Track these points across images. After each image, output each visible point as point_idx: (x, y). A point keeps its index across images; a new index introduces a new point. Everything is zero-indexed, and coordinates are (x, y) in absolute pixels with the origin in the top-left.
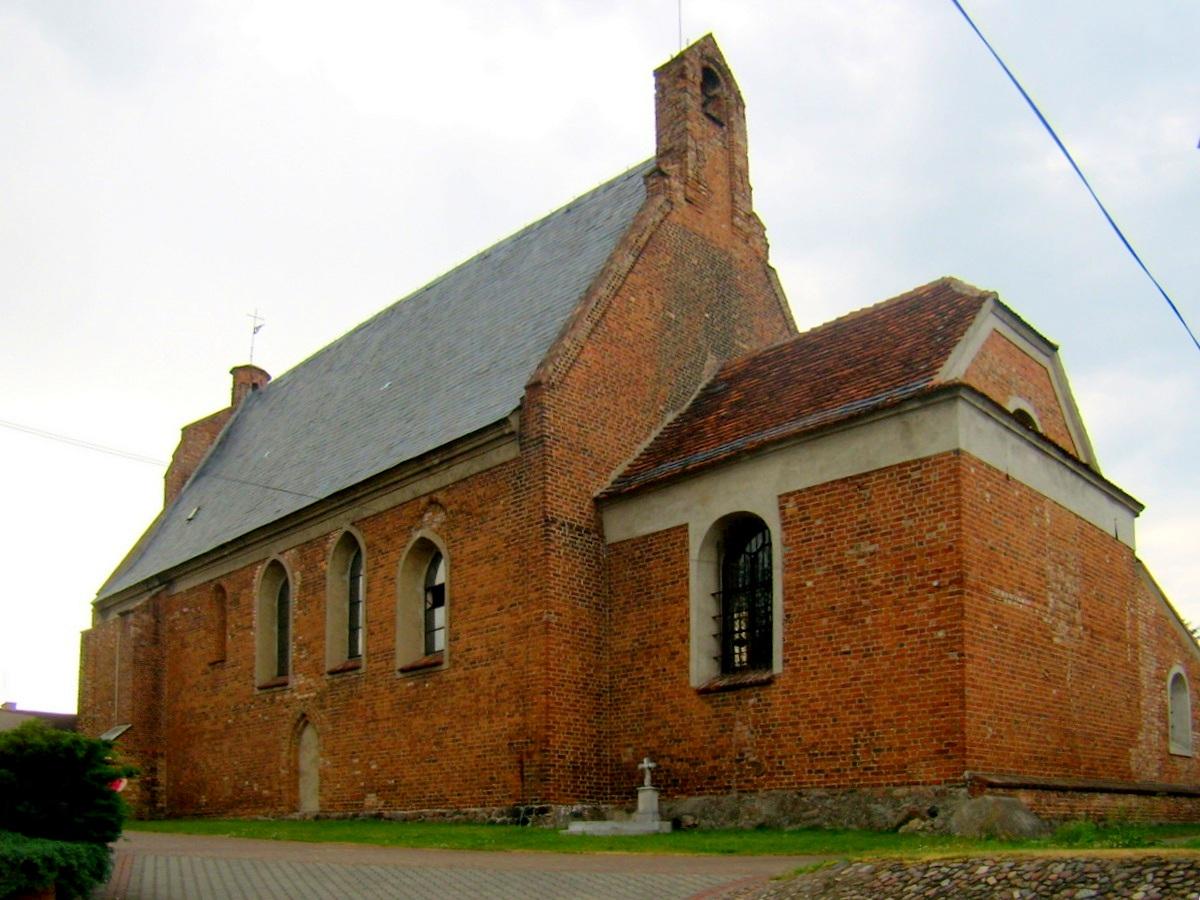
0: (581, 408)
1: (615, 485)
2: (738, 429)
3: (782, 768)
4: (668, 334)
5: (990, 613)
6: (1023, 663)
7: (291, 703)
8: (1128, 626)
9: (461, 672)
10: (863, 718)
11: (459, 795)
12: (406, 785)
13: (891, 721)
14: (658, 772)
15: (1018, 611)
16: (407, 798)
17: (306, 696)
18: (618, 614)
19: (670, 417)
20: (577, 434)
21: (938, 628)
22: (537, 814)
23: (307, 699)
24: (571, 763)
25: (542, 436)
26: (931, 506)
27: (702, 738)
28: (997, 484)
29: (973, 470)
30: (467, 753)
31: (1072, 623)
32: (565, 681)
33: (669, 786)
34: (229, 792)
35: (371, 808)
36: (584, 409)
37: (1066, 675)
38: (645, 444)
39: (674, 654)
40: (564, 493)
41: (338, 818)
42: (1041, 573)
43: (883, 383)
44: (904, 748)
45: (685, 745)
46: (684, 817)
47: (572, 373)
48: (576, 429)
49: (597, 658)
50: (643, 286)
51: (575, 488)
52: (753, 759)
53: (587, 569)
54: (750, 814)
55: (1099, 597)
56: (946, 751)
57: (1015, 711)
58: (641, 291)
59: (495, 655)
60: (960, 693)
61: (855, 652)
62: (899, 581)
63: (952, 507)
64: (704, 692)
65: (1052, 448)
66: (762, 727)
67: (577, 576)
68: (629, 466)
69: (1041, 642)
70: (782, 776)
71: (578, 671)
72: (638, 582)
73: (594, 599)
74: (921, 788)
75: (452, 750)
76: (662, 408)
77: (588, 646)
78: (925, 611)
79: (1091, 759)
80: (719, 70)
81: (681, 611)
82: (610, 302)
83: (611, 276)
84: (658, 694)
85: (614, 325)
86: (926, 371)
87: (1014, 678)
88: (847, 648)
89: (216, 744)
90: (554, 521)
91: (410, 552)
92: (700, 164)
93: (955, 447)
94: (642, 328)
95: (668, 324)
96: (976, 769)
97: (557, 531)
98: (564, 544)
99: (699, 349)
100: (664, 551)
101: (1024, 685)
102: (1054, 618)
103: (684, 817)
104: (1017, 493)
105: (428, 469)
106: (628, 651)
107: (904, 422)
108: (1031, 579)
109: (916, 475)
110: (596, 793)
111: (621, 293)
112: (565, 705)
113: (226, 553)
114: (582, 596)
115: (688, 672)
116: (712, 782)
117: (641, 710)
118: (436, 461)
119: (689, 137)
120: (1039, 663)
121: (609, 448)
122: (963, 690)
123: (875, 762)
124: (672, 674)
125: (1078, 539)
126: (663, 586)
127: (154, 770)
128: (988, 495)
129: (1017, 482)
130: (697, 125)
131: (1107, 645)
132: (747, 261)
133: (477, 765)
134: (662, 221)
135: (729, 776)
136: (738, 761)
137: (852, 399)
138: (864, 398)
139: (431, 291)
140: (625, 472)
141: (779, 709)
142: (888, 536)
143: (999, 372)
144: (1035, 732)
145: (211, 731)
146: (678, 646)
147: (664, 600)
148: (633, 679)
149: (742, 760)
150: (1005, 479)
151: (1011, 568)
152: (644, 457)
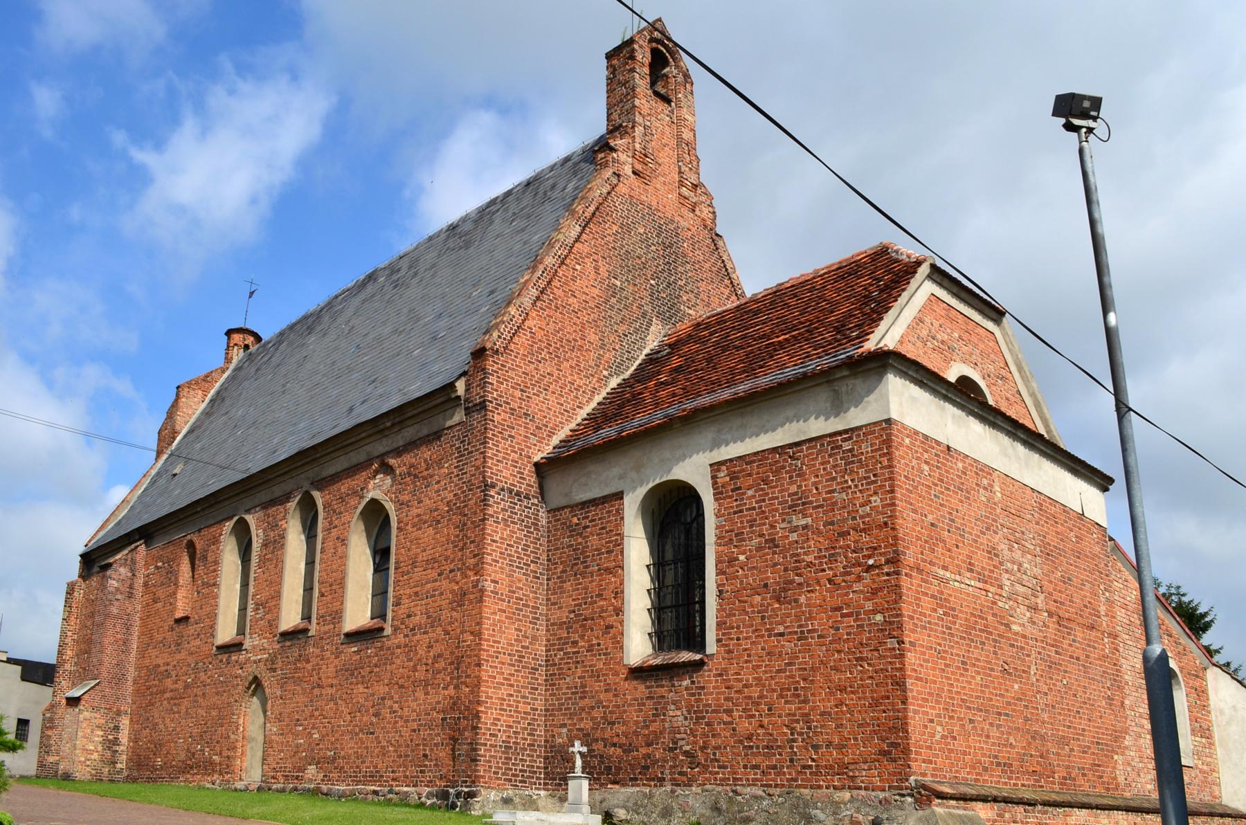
0: (524, 373)
1: (556, 450)
2: (674, 395)
3: (717, 761)
4: (613, 300)
5: (933, 596)
6: (976, 653)
7: (245, 664)
8: (1103, 613)
9: (400, 639)
10: (800, 709)
11: (393, 772)
12: (344, 758)
13: (829, 713)
14: (591, 757)
15: (968, 594)
16: (345, 772)
17: (259, 657)
18: (555, 583)
19: (614, 382)
20: (520, 399)
21: (875, 612)
22: (465, 799)
23: (260, 661)
24: (503, 742)
25: (484, 401)
26: (865, 478)
27: (636, 721)
28: (936, 455)
29: (907, 441)
30: (402, 726)
31: (1034, 608)
32: (500, 653)
33: (602, 773)
34: (183, 756)
35: (311, 781)
36: (527, 374)
37: (1029, 667)
38: (588, 409)
39: (609, 627)
40: (504, 458)
41: (277, 790)
42: (992, 552)
43: (815, 350)
44: (844, 746)
45: (619, 729)
46: (616, 810)
47: (516, 339)
48: (518, 394)
49: (533, 628)
50: (589, 255)
51: (516, 452)
52: (687, 748)
53: (525, 536)
54: (684, 812)
55: (1066, 580)
56: (890, 753)
57: (969, 708)
58: (586, 260)
59: (433, 621)
60: (900, 684)
61: (790, 633)
62: (833, 558)
63: (886, 480)
64: (640, 673)
65: (999, 417)
66: (695, 712)
67: (515, 542)
68: (571, 431)
69: (996, 628)
70: (716, 770)
71: (513, 642)
72: (574, 550)
73: (532, 566)
74: (863, 792)
75: (389, 723)
76: (605, 373)
77: (524, 616)
78: (862, 591)
79: (1068, 767)
80: (668, 51)
81: (615, 582)
82: (556, 271)
83: (557, 246)
84: (592, 671)
85: (559, 292)
86: (858, 337)
87: (967, 670)
88: (781, 629)
89: (175, 704)
90: (493, 486)
91: (361, 513)
92: (647, 138)
93: (886, 417)
94: (588, 295)
95: (613, 291)
96: (924, 775)
97: (496, 496)
98: (503, 510)
99: (644, 315)
100: (600, 519)
101: (978, 678)
102: (1011, 603)
103: (616, 810)
104: (960, 465)
105: (382, 430)
106: (565, 623)
107: (834, 391)
108: (981, 560)
109: (847, 446)
110: (529, 777)
111: (568, 261)
112: (499, 679)
113: (199, 509)
114: (520, 563)
115: (622, 647)
116: (644, 772)
117: (576, 688)
118: (388, 424)
119: (637, 113)
120: (995, 653)
121: (552, 413)
122: (904, 683)
123: (813, 760)
124: (606, 649)
125: (1036, 515)
126: (598, 555)
127: (117, 728)
128: (926, 467)
129: (960, 453)
130: (644, 101)
131: (1079, 634)
132: (694, 229)
133: (411, 741)
134: (609, 193)
135: (663, 766)
136: (671, 750)
137: (783, 366)
138: (795, 365)
139: (405, 259)
140: (567, 436)
141: (712, 693)
142: (820, 510)
143: (939, 337)
144: (994, 733)
145: (172, 691)
146: (612, 620)
147: (599, 570)
148: (569, 653)
149: (676, 749)
150: (945, 449)
151: (957, 547)
152: (587, 422)
